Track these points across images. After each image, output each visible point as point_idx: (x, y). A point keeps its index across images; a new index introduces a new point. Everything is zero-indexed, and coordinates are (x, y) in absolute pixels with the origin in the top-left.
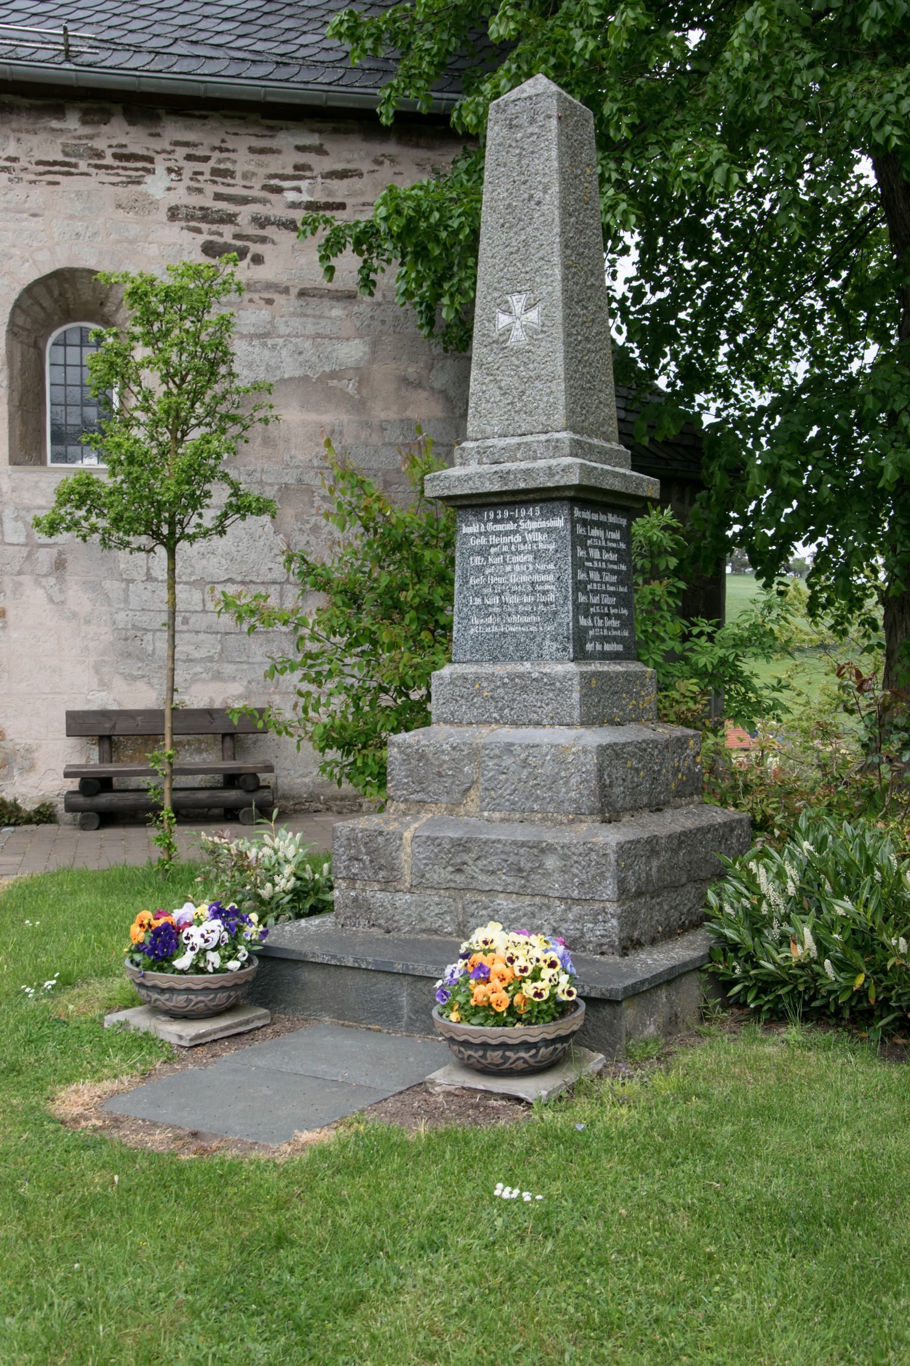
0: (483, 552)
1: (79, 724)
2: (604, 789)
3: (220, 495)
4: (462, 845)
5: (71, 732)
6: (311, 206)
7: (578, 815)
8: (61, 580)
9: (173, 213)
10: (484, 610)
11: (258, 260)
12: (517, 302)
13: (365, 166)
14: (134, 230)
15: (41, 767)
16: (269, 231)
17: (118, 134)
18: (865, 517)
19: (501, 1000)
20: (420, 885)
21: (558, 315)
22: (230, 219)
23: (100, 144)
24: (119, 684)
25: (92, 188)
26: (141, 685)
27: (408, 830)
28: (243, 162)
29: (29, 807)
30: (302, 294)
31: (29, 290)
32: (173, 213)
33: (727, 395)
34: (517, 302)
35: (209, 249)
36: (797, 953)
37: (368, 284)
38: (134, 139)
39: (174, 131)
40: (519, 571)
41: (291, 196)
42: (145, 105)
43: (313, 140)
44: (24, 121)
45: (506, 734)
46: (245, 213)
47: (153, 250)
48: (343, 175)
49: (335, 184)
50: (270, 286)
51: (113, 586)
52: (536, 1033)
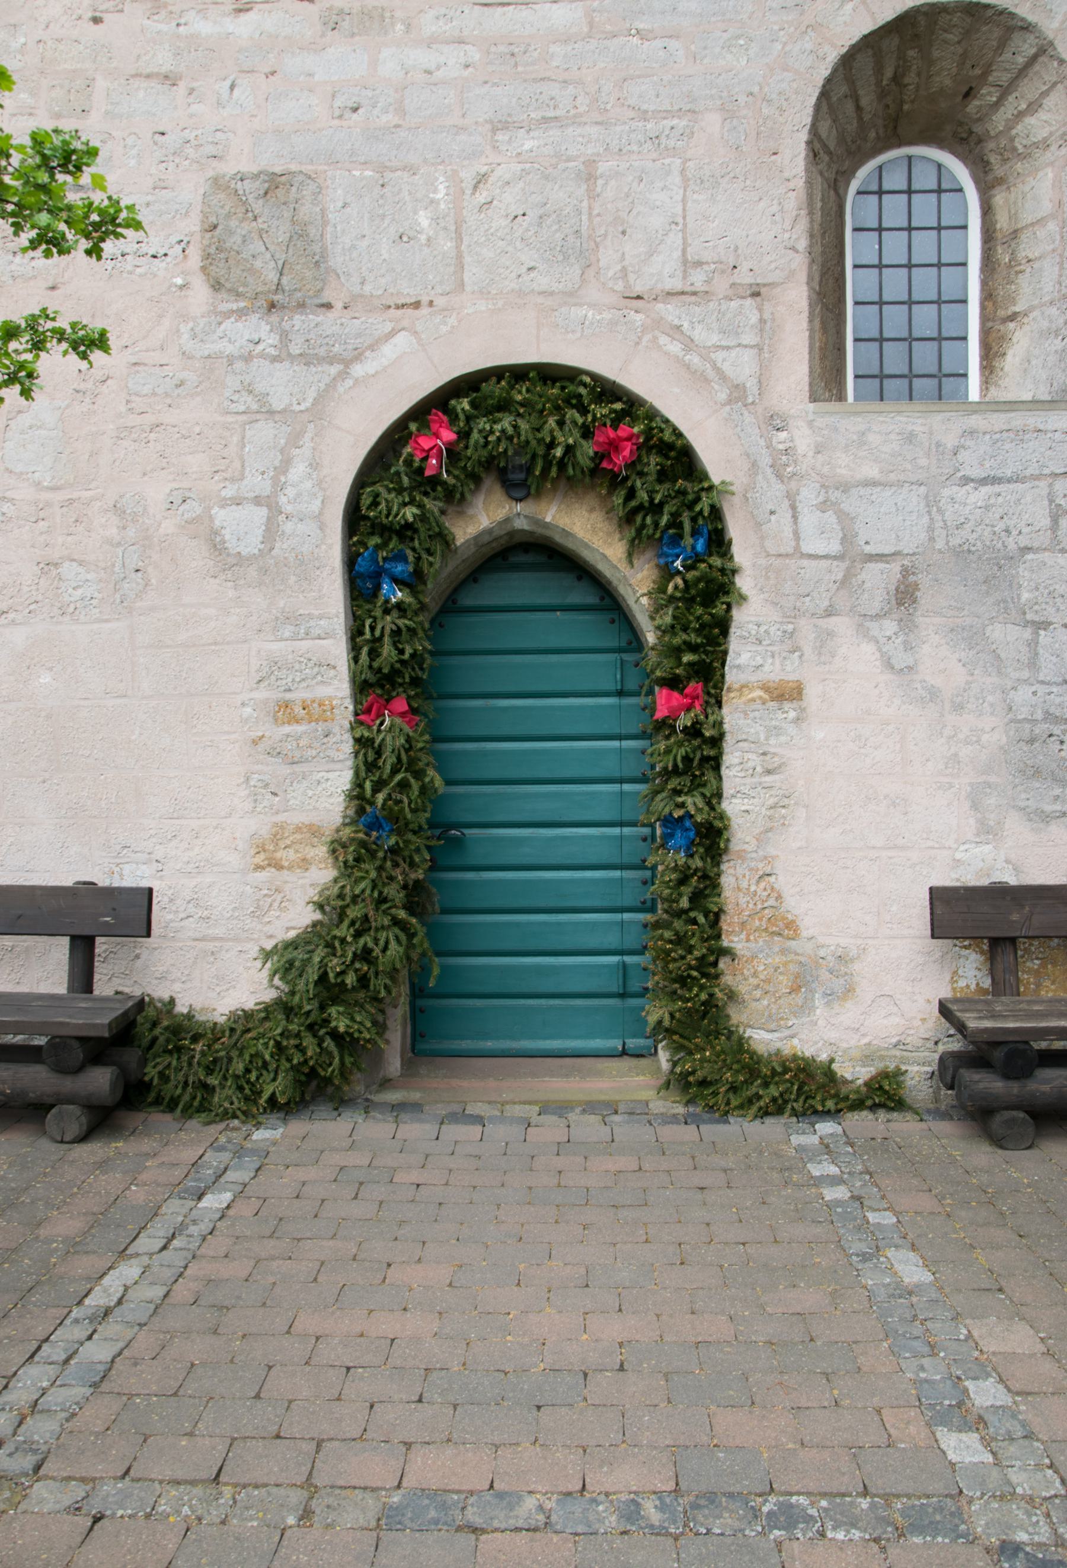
8: (907, 625)
24: (1016, 827)
29: (855, 1073)
51: (1008, 636)
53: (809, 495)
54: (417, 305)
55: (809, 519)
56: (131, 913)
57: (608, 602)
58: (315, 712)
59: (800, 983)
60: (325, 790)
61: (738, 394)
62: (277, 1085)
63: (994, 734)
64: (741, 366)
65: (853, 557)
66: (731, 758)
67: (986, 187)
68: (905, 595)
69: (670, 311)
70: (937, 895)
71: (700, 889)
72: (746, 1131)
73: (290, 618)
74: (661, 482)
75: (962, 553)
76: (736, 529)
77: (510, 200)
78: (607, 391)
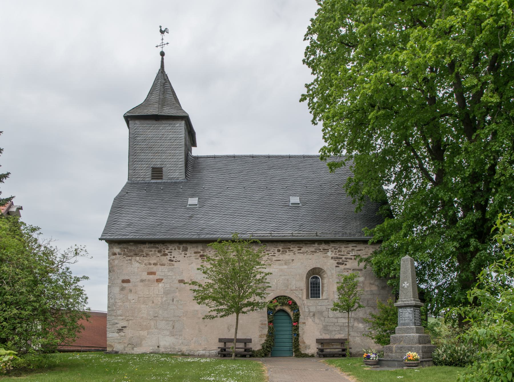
0: (402, 313)
1: (318, 341)
2: (419, 340)
3: (356, 305)
4: (401, 347)
5: (317, 342)
6: (354, 256)
7: (416, 344)
8: (314, 317)
9: (332, 258)
10: (402, 320)
11: (346, 265)
12: (406, 283)
13: (363, 249)
14: (326, 261)
15: (311, 348)
16: (348, 260)
17: (323, 246)
18: (476, 291)
19: (411, 358)
20: (396, 352)
21: (411, 284)
22: (341, 258)
23: (320, 248)
24: (323, 334)
25: (319, 255)
26: (327, 335)
27: (394, 346)
28: (343, 249)
29: (310, 355)
30: (353, 270)
31: (309, 271)
32: (332, 258)
33: (427, 283)
34: (406, 283)
35: (338, 263)
36: (443, 358)
37: (365, 268)
38: (326, 247)
39: (332, 245)
40: (407, 315)
41: (351, 254)
42: (327, 242)
43: (355, 245)
44: (309, 245)
45: (406, 334)
46: (344, 257)
47: (329, 264)
48: (360, 250)
49: (358, 252)
50: (348, 269)
51: (322, 318)
52: (415, 362)
53: (306, 307)
54: (162, 54)
55: (306, 309)
56: (250, 341)
57: (288, 315)
58: (265, 324)
59: (306, 347)
60: (266, 331)
61: (300, 298)
62: (263, 355)
63: (321, 326)
64: (300, 296)
65: (310, 312)
66: (300, 328)
67: (322, 279)
68: (314, 315)
69: (294, 291)
70: (317, 339)
71: (297, 340)
72: (300, 359)
73: (263, 316)
74: (294, 306)
75: (319, 312)
76: (300, 309)
77: (281, 282)
78: (289, 298)
